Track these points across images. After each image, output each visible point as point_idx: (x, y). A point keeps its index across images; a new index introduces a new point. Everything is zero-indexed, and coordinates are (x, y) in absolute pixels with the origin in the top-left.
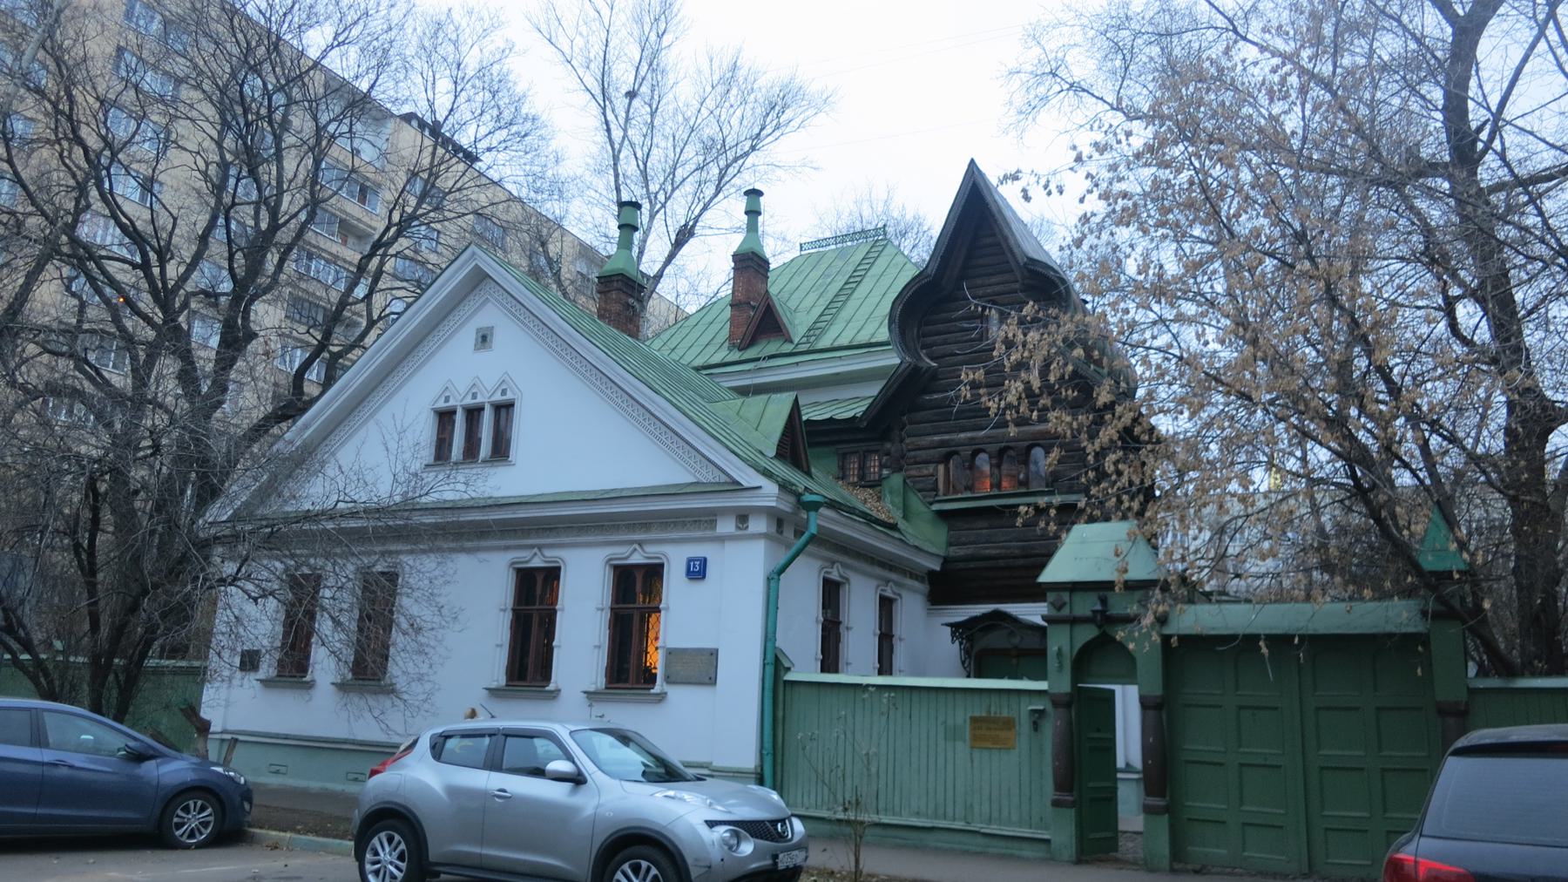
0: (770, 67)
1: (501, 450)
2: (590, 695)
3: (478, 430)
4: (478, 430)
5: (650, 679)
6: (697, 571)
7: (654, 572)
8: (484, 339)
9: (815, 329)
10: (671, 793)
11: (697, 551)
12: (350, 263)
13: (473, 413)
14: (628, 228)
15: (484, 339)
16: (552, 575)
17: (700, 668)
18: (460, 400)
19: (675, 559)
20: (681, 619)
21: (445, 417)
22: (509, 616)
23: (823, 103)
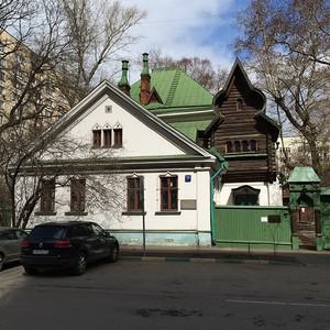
0: (141, 8)
1: (119, 143)
2: (157, 214)
3: (114, 136)
4: (114, 136)
5: (176, 208)
6: (188, 179)
7: (175, 179)
8: (109, 109)
9: (170, 98)
10: (170, 244)
11: (188, 173)
12: (208, 107)
13: (108, 132)
14: (125, 69)
15: (109, 109)
16: (140, 180)
17: (191, 205)
18: (103, 127)
19: (181, 176)
20: (184, 191)
21: (97, 133)
22: (159, 192)
23: (144, 15)
